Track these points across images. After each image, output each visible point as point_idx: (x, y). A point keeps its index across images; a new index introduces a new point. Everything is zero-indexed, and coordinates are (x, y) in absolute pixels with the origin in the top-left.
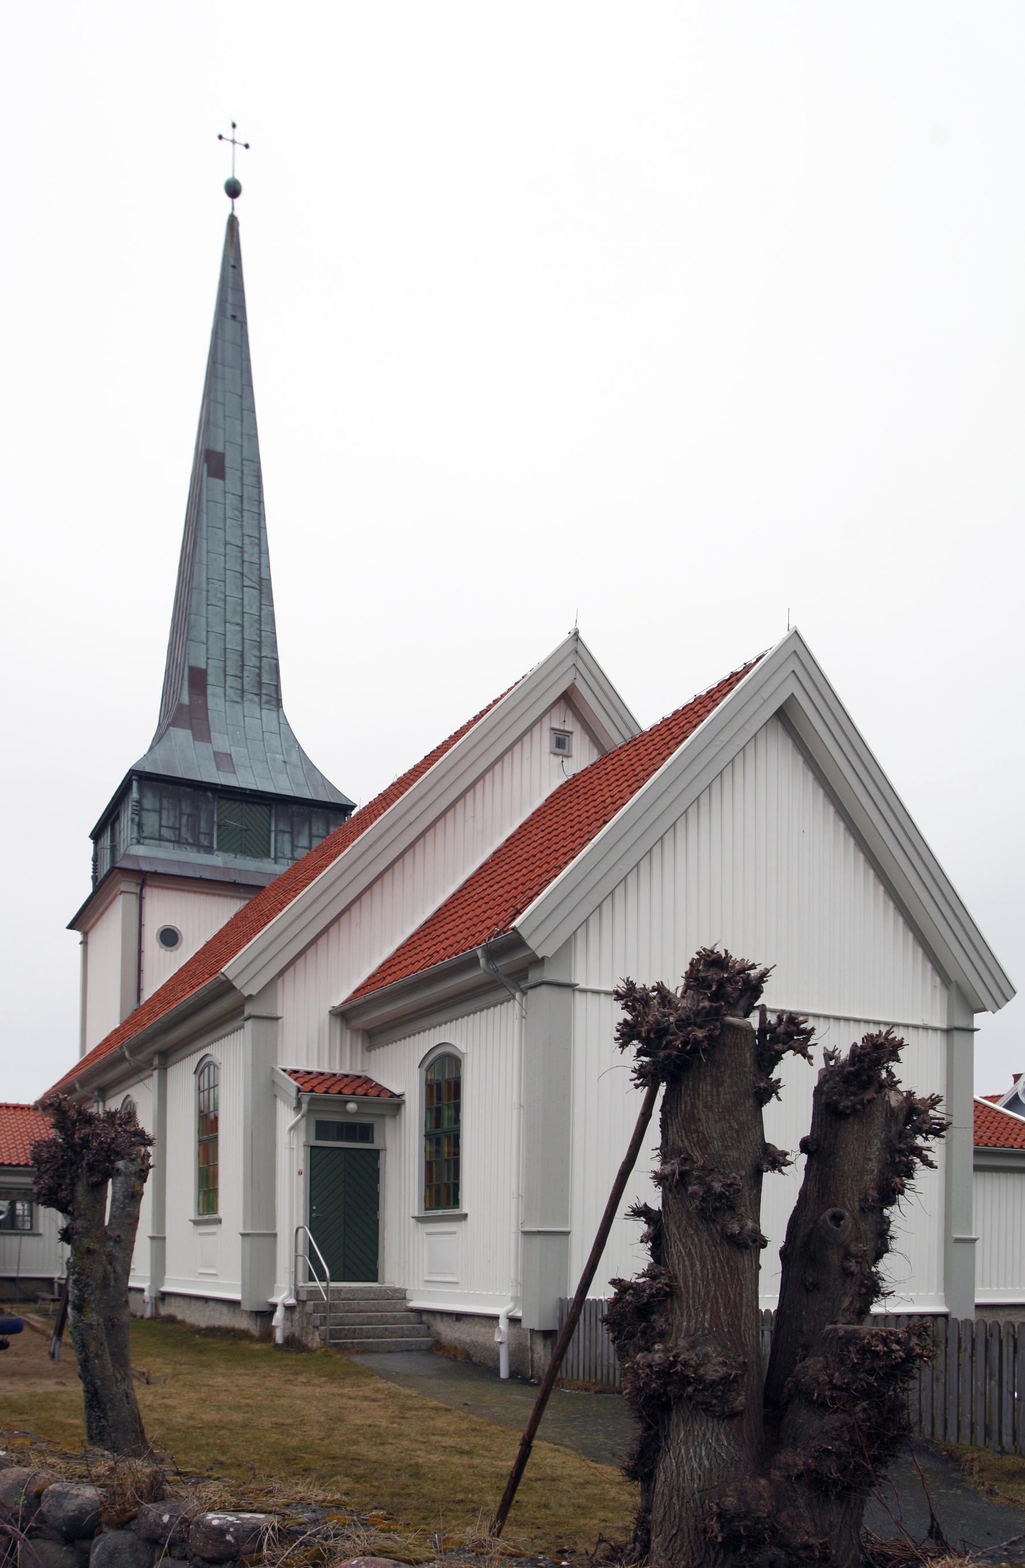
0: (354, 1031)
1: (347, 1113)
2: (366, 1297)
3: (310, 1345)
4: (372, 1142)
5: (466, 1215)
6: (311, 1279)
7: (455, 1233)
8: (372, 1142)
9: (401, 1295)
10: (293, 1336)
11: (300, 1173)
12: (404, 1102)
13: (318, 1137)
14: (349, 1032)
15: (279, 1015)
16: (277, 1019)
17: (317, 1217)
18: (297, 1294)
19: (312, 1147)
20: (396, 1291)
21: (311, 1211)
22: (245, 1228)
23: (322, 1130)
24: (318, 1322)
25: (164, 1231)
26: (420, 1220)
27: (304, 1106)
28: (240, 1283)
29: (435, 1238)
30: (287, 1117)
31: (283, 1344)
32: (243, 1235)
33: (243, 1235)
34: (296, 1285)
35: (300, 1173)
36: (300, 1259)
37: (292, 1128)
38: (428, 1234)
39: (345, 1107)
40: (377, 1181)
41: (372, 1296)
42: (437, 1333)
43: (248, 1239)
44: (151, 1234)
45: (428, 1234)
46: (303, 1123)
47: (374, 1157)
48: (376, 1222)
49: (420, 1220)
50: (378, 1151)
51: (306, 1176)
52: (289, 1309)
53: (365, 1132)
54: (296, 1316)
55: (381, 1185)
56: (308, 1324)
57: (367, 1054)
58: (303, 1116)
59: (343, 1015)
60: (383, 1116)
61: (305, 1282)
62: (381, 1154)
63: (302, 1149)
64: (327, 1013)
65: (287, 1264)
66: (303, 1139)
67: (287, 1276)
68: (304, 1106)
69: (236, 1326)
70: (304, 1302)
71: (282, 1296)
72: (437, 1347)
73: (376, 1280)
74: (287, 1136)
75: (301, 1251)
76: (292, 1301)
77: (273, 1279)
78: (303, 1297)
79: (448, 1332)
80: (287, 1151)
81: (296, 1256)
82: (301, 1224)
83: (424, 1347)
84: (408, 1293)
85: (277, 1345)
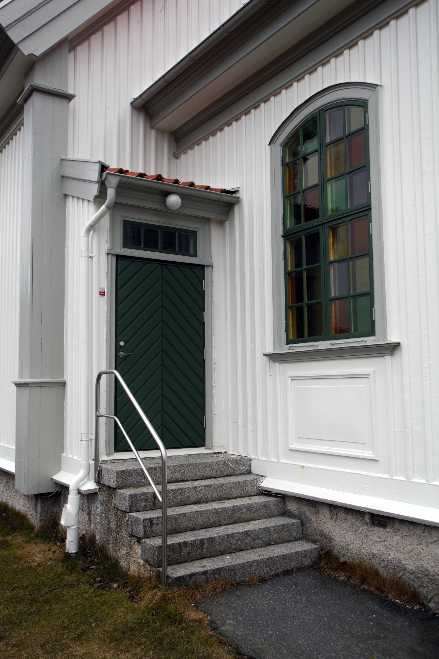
0: (160, 132)
1: (167, 212)
2: (200, 474)
3: (123, 563)
4: (195, 255)
5: (398, 345)
6: (120, 445)
7: (366, 376)
8: (195, 255)
9: (243, 466)
10: (93, 538)
11: (102, 293)
12: (238, 200)
13: (126, 245)
14: (153, 132)
15: (70, 91)
16: (69, 98)
17: (126, 357)
18: (99, 475)
19: (119, 257)
20: (239, 461)
21: (118, 348)
22: (21, 375)
23: (134, 234)
24: (140, 530)
25: (62, 373)
26: (274, 358)
27: (111, 193)
28: (14, 447)
29: (301, 385)
30: (82, 215)
31: (76, 553)
32: (18, 385)
33: (18, 385)
34: (96, 459)
35: (102, 293)
36: (102, 420)
37: (92, 227)
38: (294, 379)
39: (164, 202)
40: (202, 308)
41: (208, 473)
42: (322, 535)
43: (26, 391)
44: (270, 350)
45: (294, 379)
46: (106, 222)
47: (199, 272)
48: (202, 364)
49: (274, 358)
50: (202, 267)
51: (110, 298)
52: (88, 498)
53: (182, 240)
54: (98, 507)
55: (206, 313)
56: (118, 526)
57: (174, 160)
58: (108, 208)
59: (148, 107)
60: (208, 220)
61: (108, 454)
62: (207, 271)
63: (104, 259)
64: (127, 108)
65: (83, 428)
66: (106, 245)
67: (83, 446)
68: (111, 193)
69: (10, 503)
70: (111, 490)
71: (76, 476)
72: (328, 564)
73: (202, 444)
74: (83, 241)
75: (103, 411)
76: (90, 486)
77: (59, 444)
78: (110, 481)
79: (350, 541)
80: (84, 261)
81: (97, 417)
82: (104, 368)
83: (307, 563)
84: (253, 463)
85: (68, 556)
